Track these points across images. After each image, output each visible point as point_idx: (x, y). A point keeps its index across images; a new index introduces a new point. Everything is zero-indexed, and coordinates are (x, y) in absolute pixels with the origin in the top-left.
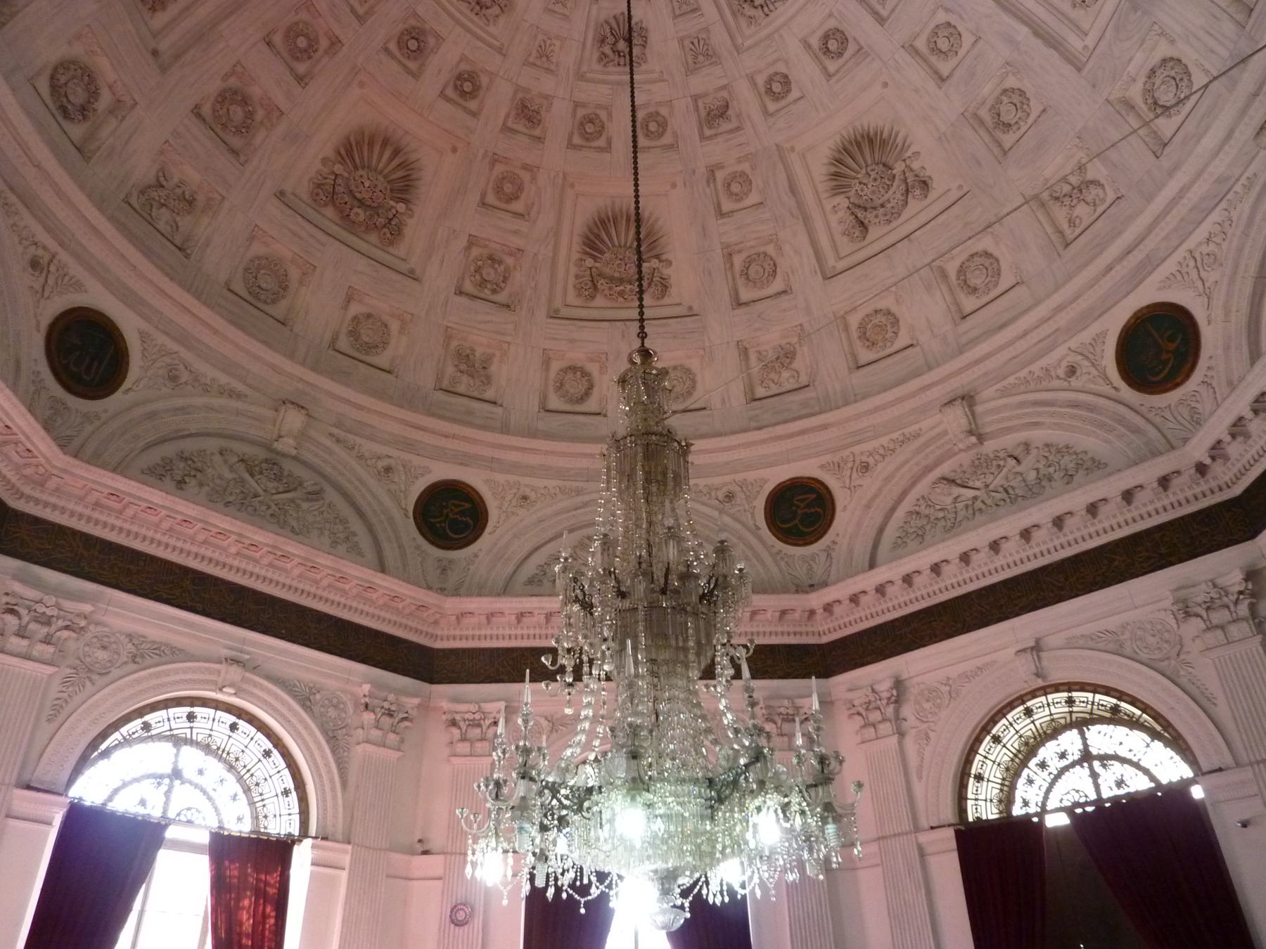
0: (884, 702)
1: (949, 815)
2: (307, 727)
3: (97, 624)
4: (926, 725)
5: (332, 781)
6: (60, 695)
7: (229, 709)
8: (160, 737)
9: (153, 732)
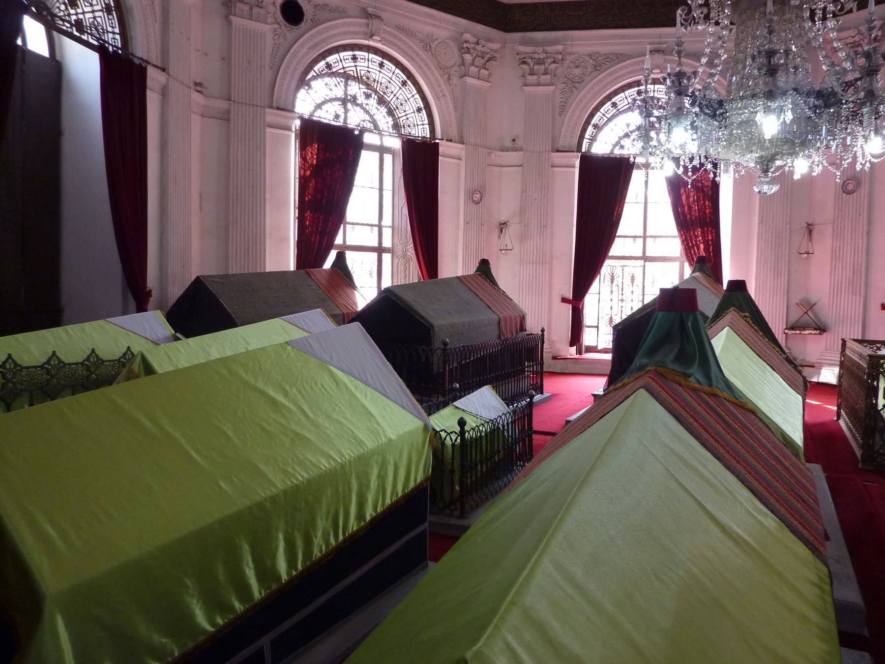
3: (570, 54)
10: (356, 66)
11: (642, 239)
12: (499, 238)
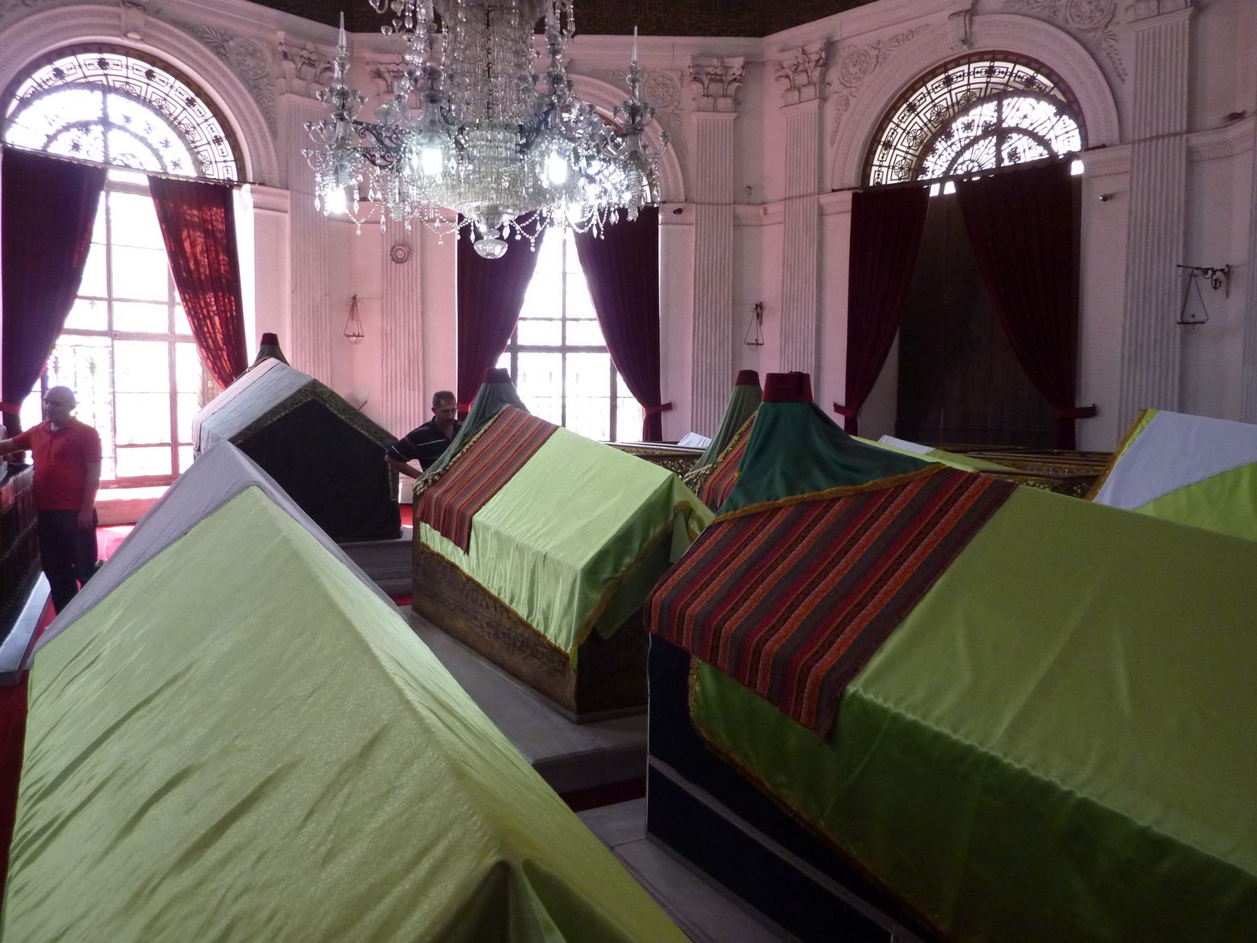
0: (812, 64)
1: (852, 179)
2: (225, 76)
4: (849, 90)
5: (260, 129)
7: (141, 55)
9: (68, 79)
10: (106, 75)
11: (105, 304)
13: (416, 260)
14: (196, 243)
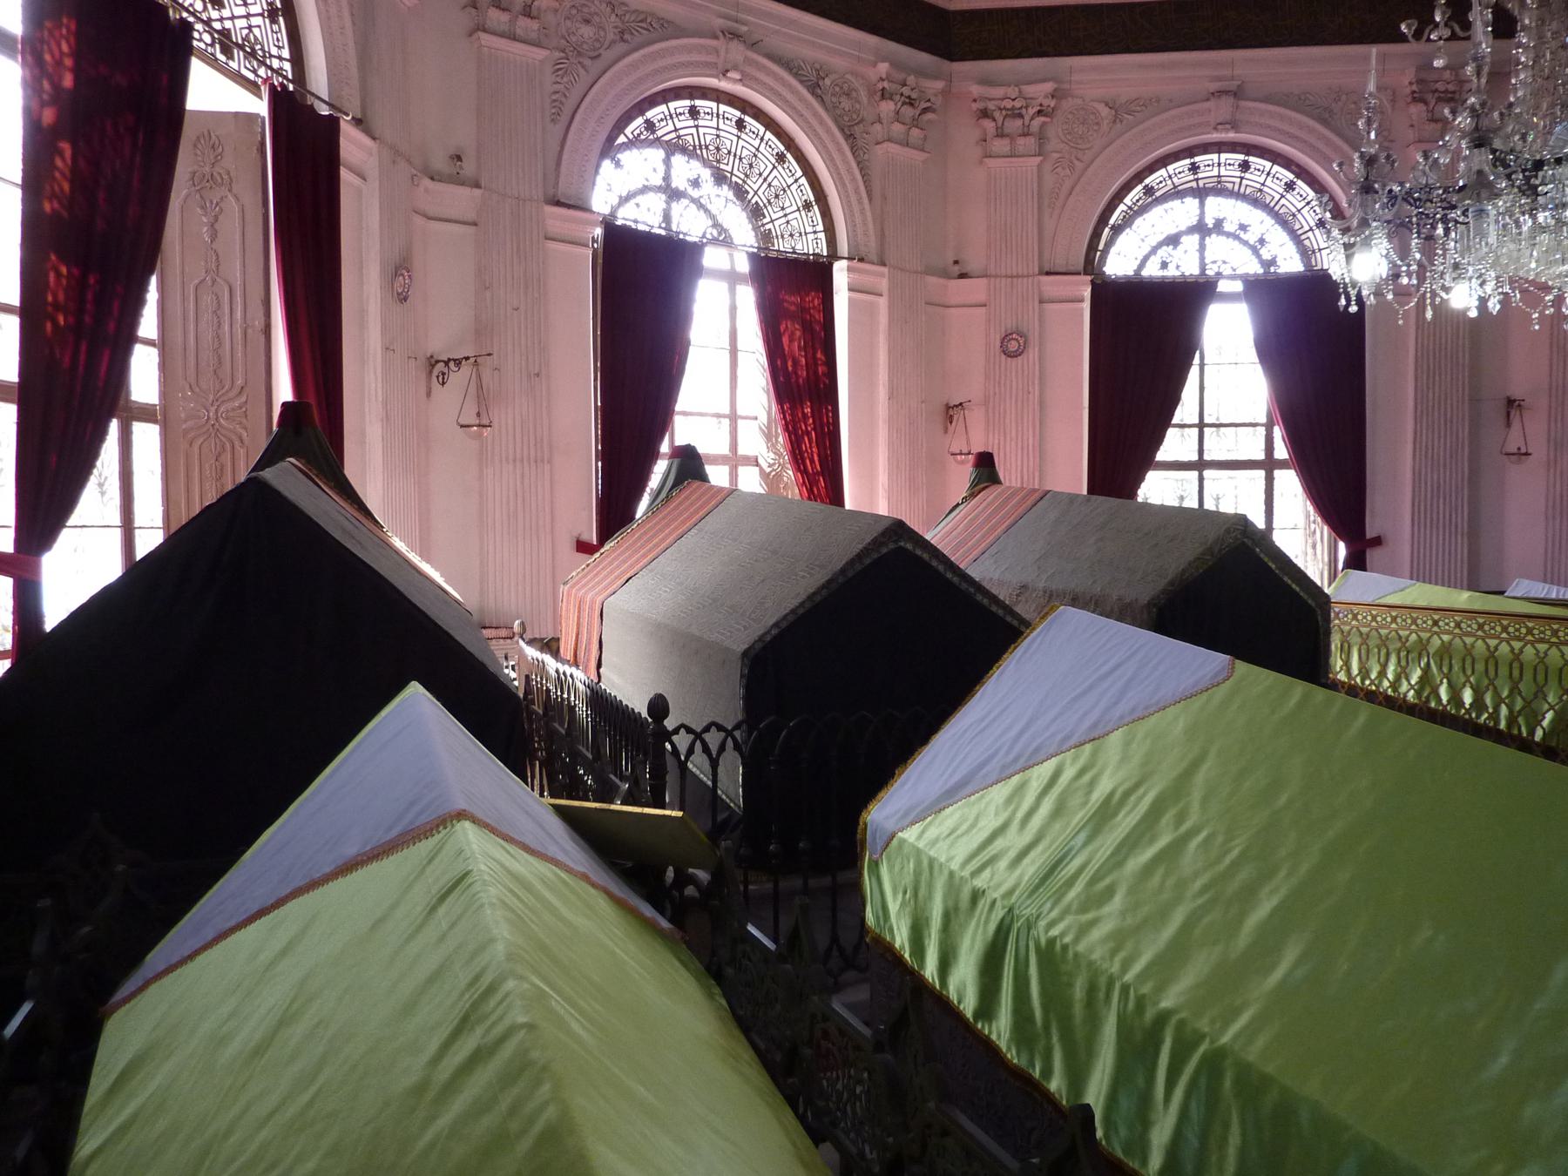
2: (822, 122)
6: (557, 87)
8: (1166, 198)
9: (1158, 194)
10: (697, 127)
11: (1195, 431)
12: (946, 431)
13: (1032, 353)
14: (793, 344)
